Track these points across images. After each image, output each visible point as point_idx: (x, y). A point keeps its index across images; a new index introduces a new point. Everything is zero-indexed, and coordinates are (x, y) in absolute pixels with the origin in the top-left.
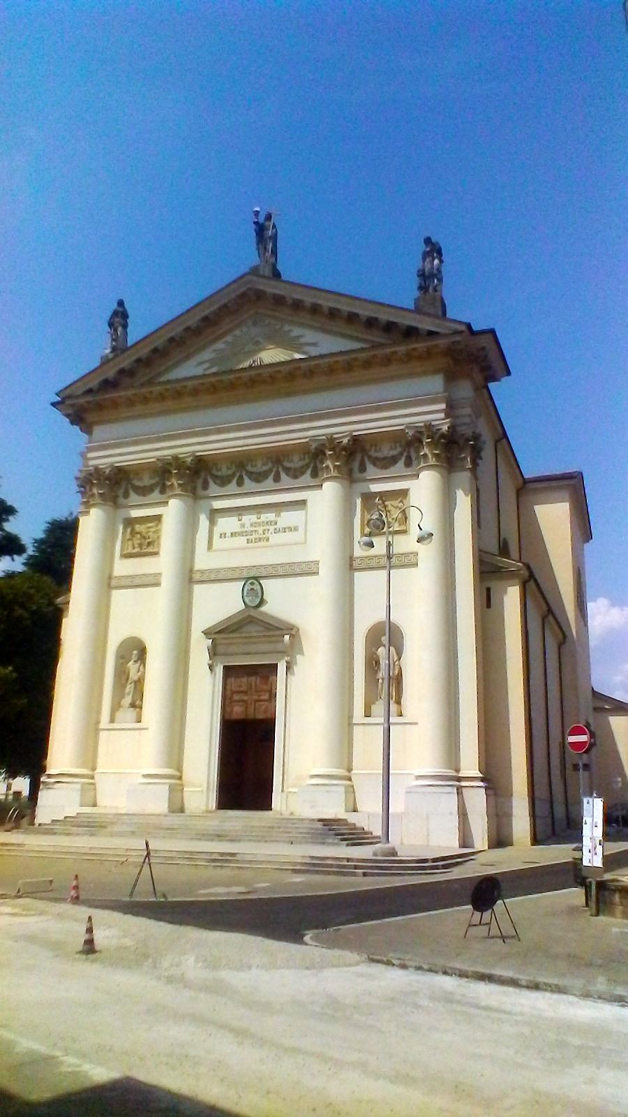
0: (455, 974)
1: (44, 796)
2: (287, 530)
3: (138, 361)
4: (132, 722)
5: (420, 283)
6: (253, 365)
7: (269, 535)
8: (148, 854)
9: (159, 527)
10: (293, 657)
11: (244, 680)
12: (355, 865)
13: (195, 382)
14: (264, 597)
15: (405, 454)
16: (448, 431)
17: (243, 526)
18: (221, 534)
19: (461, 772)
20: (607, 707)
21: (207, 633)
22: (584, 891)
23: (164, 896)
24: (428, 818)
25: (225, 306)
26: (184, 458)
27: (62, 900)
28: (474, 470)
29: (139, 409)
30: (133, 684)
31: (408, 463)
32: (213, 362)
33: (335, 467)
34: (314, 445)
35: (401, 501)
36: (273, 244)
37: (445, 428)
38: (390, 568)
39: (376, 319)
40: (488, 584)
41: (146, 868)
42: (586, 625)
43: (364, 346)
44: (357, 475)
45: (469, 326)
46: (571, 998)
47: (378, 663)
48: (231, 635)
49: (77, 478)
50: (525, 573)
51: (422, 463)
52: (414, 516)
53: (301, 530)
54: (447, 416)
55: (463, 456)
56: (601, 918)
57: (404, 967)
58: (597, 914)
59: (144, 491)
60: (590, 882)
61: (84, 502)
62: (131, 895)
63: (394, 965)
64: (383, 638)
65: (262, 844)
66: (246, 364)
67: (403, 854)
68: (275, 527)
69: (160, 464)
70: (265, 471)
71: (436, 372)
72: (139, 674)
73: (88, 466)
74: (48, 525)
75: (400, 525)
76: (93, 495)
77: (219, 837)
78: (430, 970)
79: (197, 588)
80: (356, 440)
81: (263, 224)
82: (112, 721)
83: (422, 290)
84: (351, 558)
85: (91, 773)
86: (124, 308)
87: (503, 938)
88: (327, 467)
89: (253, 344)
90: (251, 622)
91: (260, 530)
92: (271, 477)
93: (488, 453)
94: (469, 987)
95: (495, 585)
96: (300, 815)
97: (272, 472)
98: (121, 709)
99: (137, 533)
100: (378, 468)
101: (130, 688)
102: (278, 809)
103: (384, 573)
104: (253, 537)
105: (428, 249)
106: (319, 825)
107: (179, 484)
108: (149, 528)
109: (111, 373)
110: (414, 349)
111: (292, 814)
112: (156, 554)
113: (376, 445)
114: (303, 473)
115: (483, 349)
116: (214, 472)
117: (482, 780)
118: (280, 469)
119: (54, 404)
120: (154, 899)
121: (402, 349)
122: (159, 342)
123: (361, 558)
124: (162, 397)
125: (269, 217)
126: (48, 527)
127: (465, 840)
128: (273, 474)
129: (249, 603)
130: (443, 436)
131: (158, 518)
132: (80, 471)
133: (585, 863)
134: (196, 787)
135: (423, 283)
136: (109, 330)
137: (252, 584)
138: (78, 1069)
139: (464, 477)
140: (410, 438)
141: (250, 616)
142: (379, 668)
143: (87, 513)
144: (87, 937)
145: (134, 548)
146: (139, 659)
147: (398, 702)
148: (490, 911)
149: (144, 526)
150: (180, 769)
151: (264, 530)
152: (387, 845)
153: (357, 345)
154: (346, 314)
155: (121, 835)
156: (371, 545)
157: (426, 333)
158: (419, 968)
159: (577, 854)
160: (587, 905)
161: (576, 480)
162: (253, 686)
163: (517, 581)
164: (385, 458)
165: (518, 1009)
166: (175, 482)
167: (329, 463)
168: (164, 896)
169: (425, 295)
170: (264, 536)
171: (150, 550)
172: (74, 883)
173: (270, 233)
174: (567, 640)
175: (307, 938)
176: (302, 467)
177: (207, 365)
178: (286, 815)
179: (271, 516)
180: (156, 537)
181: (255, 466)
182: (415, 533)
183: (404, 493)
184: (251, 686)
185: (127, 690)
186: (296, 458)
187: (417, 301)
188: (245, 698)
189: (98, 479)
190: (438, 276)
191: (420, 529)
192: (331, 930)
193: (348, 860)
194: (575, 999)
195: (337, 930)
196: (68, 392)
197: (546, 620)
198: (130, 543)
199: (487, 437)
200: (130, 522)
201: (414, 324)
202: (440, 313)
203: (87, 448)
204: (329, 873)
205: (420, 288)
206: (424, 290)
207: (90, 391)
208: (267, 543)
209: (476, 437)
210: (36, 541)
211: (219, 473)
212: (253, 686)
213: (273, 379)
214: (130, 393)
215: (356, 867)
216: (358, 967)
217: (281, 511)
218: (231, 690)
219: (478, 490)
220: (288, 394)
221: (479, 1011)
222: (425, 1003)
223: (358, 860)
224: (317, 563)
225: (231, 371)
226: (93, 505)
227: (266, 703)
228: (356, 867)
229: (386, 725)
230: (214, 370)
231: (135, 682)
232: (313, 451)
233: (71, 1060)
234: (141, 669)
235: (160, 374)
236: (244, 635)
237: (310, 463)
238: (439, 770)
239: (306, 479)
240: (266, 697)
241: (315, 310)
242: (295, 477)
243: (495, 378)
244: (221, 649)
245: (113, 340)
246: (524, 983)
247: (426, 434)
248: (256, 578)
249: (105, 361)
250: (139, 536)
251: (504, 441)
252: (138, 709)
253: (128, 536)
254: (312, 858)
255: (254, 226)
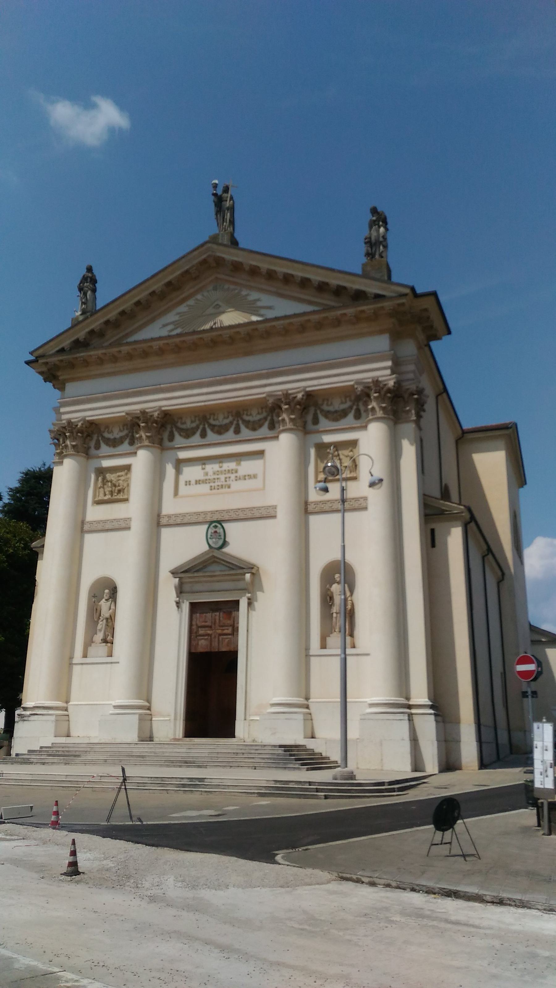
0: (423, 891)
1: (20, 729)
2: (247, 478)
3: (107, 322)
4: (105, 657)
5: (367, 250)
6: (214, 327)
7: (231, 482)
8: (125, 780)
9: (128, 476)
10: (253, 592)
11: (209, 615)
12: (317, 788)
13: (161, 343)
14: (227, 540)
15: (355, 407)
16: (394, 386)
17: (207, 474)
18: (186, 482)
19: (411, 700)
20: (543, 640)
21: (174, 573)
22: (535, 811)
23: (140, 820)
24: (381, 745)
25: (187, 272)
26: (385, 381)
27: (45, 825)
28: (417, 422)
29: (108, 367)
30: (105, 621)
31: (358, 416)
32: (176, 324)
33: (291, 420)
34: (271, 400)
35: (351, 451)
36: (231, 215)
37: (391, 383)
38: (345, 511)
39: (327, 284)
40: (433, 526)
41: (123, 791)
42: (522, 563)
43: (316, 308)
44: (310, 426)
45: (413, 289)
46: (534, 912)
47: (331, 598)
48: (196, 574)
49: (50, 431)
50: (467, 515)
51: (281, 426)
52: (364, 465)
53: (260, 476)
54: (393, 373)
55: (408, 408)
56: (552, 836)
57: (373, 884)
58: (550, 834)
59: (114, 443)
60: (542, 803)
61: (57, 453)
62: (108, 820)
63: (363, 882)
64: (337, 576)
65: (228, 770)
66: (207, 327)
67: (361, 778)
68: (236, 475)
69: (129, 418)
70: (226, 425)
71: (381, 332)
72: (111, 611)
73: (61, 420)
74: (22, 475)
75: (351, 472)
76: (66, 446)
77: (187, 763)
78: (398, 887)
79: (165, 532)
80: (309, 395)
81: (221, 196)
82: (85, 656)
83: (369, 256)
84: (306, 503)
85: (65, 705)
86: (92, 273)
87: (464, 856)
88: (283, 420)
89: (214, 307)
90: (214, 562)
91: (222, 477)
92: (232, 430)
93: (430, 405)
94: (437, 902)
95: (439, 527)
96: (261, 742)
97: (232, 424)
98: (93, 645)
99: (108, 481)
100: (330, 420)
101: (101, 625)
102: (242, 737)
103: (339, 516)
104: (216, 484)
105: (374, 218)
106: (280, 751)
107: (147, 436)
108: (119, 476)
109: (81, 335)
110: (363, 311)
111: (254, 741)
112: (127, 500)
113: (328, 400)
114: (261, 426)
115: (426, 310)
116: (179, 425)
117: (432, 707)
118: (240, 422)
119: (28, 363)
120: (131, 823)
121: (350, 311)
122: (127, 305)
123: (316, 503)
124: (130, 357)
125: (226, 190)
126: (22, 477)
127: (417, 765)
128: (233, 426)
129: (213, 545)
130: (389, 391)
131: (127, 468)
132: (53, 424)
133: (537, 785)
134: (164, 716)
135: (369, 249)
136: (79, 294)
137: (216, 527)
138: (76, 984)
139: (409, 428)
140: (358, 393)
141: (214, 557)
142: (333, 604)
143: (61, 463)
144: (71, 859)
145: (105, 495)
146: (110, 597)
147: (352, 635)
148: (451, 830)
149: (114, 475)
150: (149, 701)
151: (226, 478)
152: (346, 769)
153: (309, 308)
154: (299, 279)
155: (93, 763)
156: (326, 490)
157: (373, 296)
158: (388, 886)
159: (528, 777)
160: (539, 825)
161: (511, 430)
162: (217, 621)
163: (459, 523)
164: (336, 412)
165: (485, 923)
166: (143, 434)
167: (285, 416)
168: (140, 820)
169: (372, 260)
170: (226, 483)
171: (120, 496)
172: (55, 809)
173: (228, 204)
174: (505, 578)
175: (278, 858)
176: (260, 420)
177: (171, 327)
178: (249, 741)
179: (232, 465)
180: (125, 485)
181: (217, 419)
182: (365, 478)
183: (353, 444)
184: (215, 621)
185: (99, 627)
186: (254, 412)
187: (364, 266)
188: (209, 632)
189: (72, 432)
190: (384, 243)
191: (372, 475)
192: (300, 850)
193: (310, 783)
194: (539, 913)
195: (306, 850)
196: (40, 352)
197: (486, 558)
198: (102, 490)
199: (430, 392)
200: (101, 472)
201: (363, 288)
202: (386, 278)
203: (59, 403)
204: (293, 796)
205: (368, 254)
206: (371, 256)
207: (62, 351)
208: (229, 490)
209: (420, 392)
210: (11, 490)
211: (184, 426)
212: (217, 621)
213: (232, 340)
214: (100, 352)
215: (317, 790)
216: (330, 884)
217: (241, 460)
218: (197, 625)
219: (421, 441)
220: (248, 353)
221: (449, 926)
222: (397, 918)
223: (320, 784)
224: (275, 507)
225: (194, 332)
226: (66, 456)
227: (230, 636)
228: (317, 790)
229: (343, 656)
230: (179, 331)
231: (107, 619)
232: (270, 405)
233: (69, 975)
234: (113, 607)
235: (128, 335)
236: (207, 574)
237: (268, 415)
238: (387, 698)
239: (264, 430)
240: (229, 631)
241: (271, 275)
242: (254, 429)
243: (436, 337)
244: (186, 587)
245: (83, 303)
246: (488, 898)
247: (374, 388)
248: (219, 522)
249: (76, 323)
250: (110, 484)
251: (445, 395)
252: (109, 644)
253: (100, 484)
254: (276, 781)
255: (213, 198)
